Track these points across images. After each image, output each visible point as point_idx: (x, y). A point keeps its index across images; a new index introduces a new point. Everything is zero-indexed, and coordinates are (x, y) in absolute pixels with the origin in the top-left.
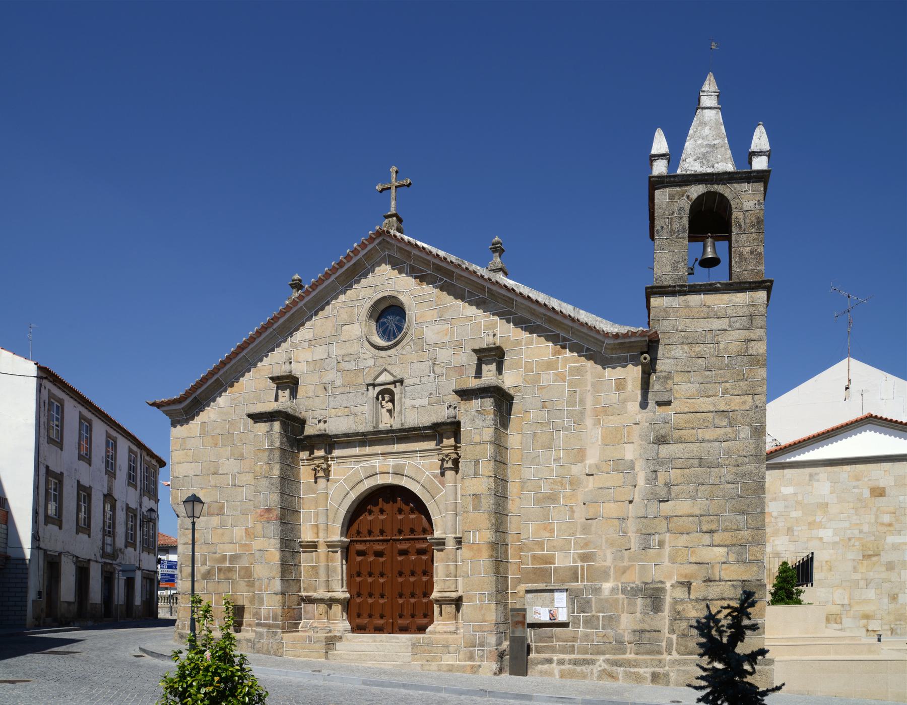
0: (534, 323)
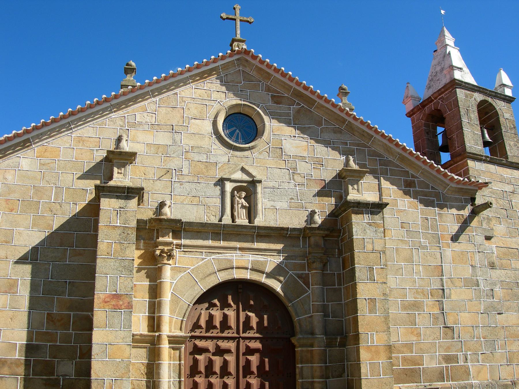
0: (387, 158)
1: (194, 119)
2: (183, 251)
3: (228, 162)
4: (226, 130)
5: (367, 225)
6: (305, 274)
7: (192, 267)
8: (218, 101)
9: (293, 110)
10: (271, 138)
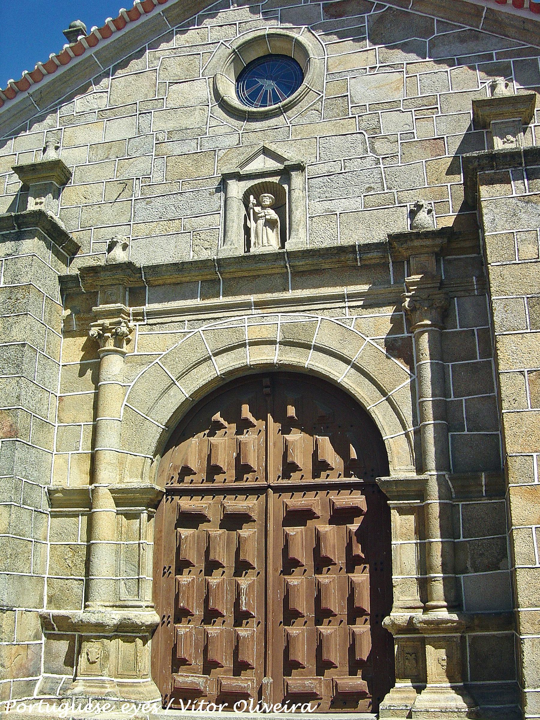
1: (176, 83)
2: (147, 324)
3: (237, 144)
4: (243, 91)
5: (519, 204)
6: (402, 338)
7: (164, 353)
8: (221, 41)
9: (368, 21)
10: (325, 81)
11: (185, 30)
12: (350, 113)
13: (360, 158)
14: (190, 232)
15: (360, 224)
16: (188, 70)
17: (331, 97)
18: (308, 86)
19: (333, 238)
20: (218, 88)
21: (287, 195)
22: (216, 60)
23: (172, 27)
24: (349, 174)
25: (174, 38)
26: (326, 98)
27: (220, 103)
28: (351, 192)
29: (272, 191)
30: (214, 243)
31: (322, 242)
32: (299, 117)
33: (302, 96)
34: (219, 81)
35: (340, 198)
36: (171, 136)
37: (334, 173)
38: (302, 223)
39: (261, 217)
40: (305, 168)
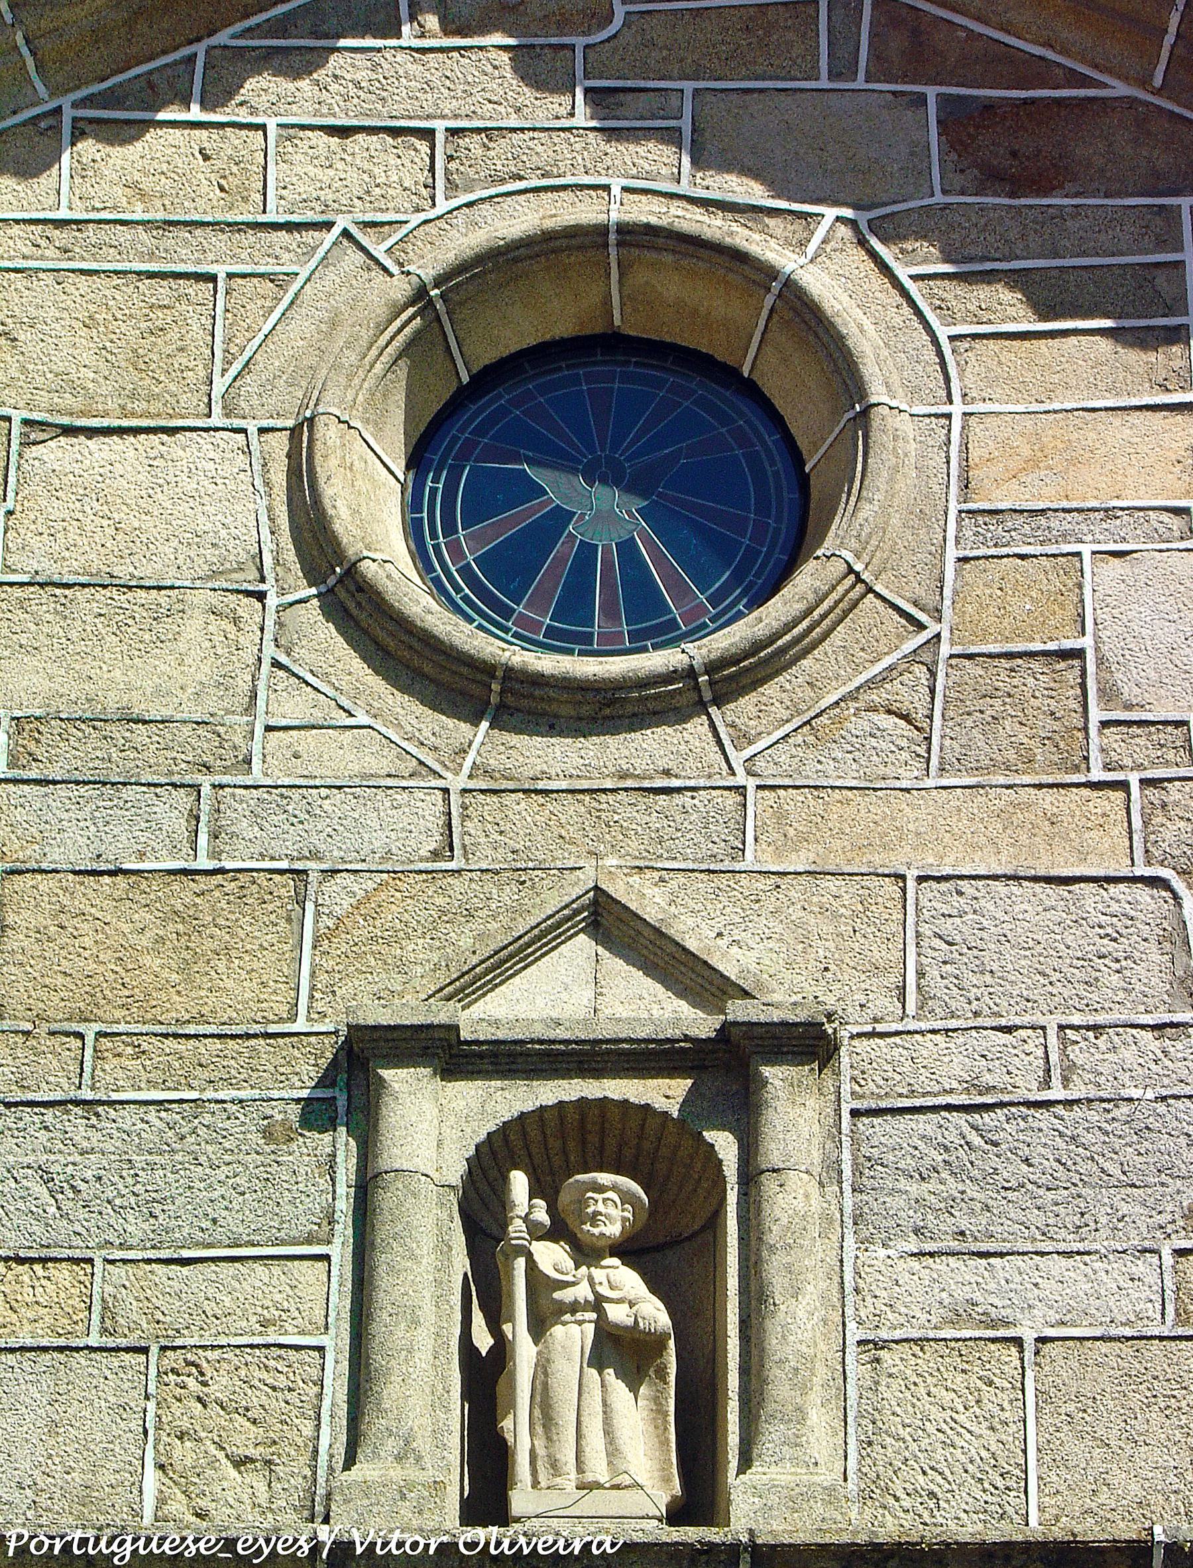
3: (436, 855)
4: (450, 529)
8: (342, 222)
10: (952, 553)
11: (128, 122)
12: (1094, 754)
13: (1154, 1027)
14: (145, 1350)
15: (1155, 1416)
16: (139, 363)
17: (984, 649)
18: (858, 567)
19: (1000, 1483)
20: (327, 503)
21: (732, 1197)
22: (308, 328)
23: (52, 95)
24: (1093, 1116)
25: (66, 157)
26: (958, 650)
27: (331, 591)
28: (1103, 1220)
29: (628, 1153)
30: (292, 1434)
31: (932, 1494)
32: (799, 739)
33: (818, 623)
34: (333, 462)
35: (1042, 1247)
36: (32, 746)
37: (1006, 1098)
38: (822, 1373)
39: (574, 1307)
40: (837, 1049)
